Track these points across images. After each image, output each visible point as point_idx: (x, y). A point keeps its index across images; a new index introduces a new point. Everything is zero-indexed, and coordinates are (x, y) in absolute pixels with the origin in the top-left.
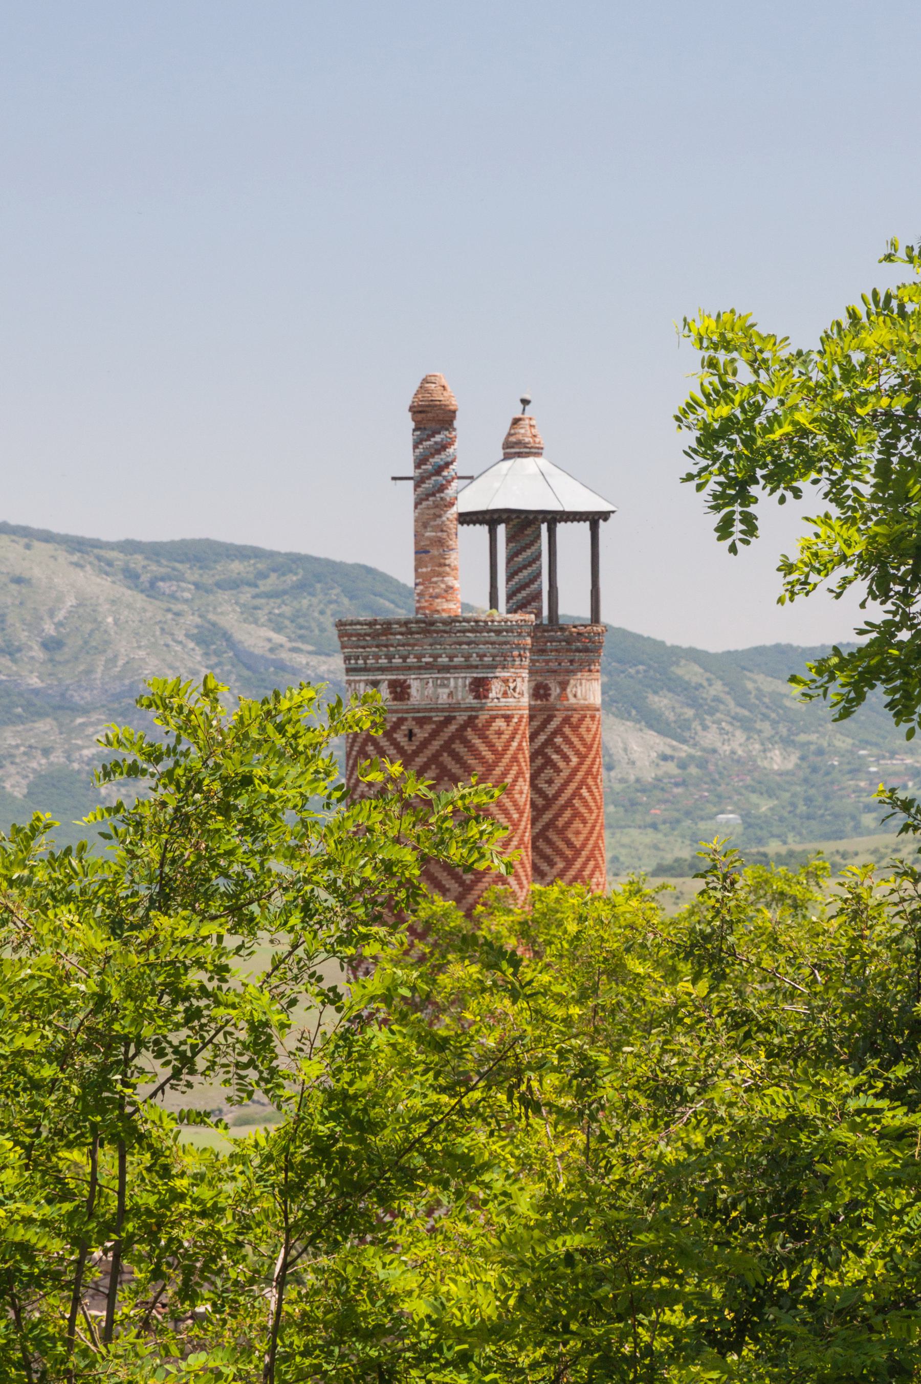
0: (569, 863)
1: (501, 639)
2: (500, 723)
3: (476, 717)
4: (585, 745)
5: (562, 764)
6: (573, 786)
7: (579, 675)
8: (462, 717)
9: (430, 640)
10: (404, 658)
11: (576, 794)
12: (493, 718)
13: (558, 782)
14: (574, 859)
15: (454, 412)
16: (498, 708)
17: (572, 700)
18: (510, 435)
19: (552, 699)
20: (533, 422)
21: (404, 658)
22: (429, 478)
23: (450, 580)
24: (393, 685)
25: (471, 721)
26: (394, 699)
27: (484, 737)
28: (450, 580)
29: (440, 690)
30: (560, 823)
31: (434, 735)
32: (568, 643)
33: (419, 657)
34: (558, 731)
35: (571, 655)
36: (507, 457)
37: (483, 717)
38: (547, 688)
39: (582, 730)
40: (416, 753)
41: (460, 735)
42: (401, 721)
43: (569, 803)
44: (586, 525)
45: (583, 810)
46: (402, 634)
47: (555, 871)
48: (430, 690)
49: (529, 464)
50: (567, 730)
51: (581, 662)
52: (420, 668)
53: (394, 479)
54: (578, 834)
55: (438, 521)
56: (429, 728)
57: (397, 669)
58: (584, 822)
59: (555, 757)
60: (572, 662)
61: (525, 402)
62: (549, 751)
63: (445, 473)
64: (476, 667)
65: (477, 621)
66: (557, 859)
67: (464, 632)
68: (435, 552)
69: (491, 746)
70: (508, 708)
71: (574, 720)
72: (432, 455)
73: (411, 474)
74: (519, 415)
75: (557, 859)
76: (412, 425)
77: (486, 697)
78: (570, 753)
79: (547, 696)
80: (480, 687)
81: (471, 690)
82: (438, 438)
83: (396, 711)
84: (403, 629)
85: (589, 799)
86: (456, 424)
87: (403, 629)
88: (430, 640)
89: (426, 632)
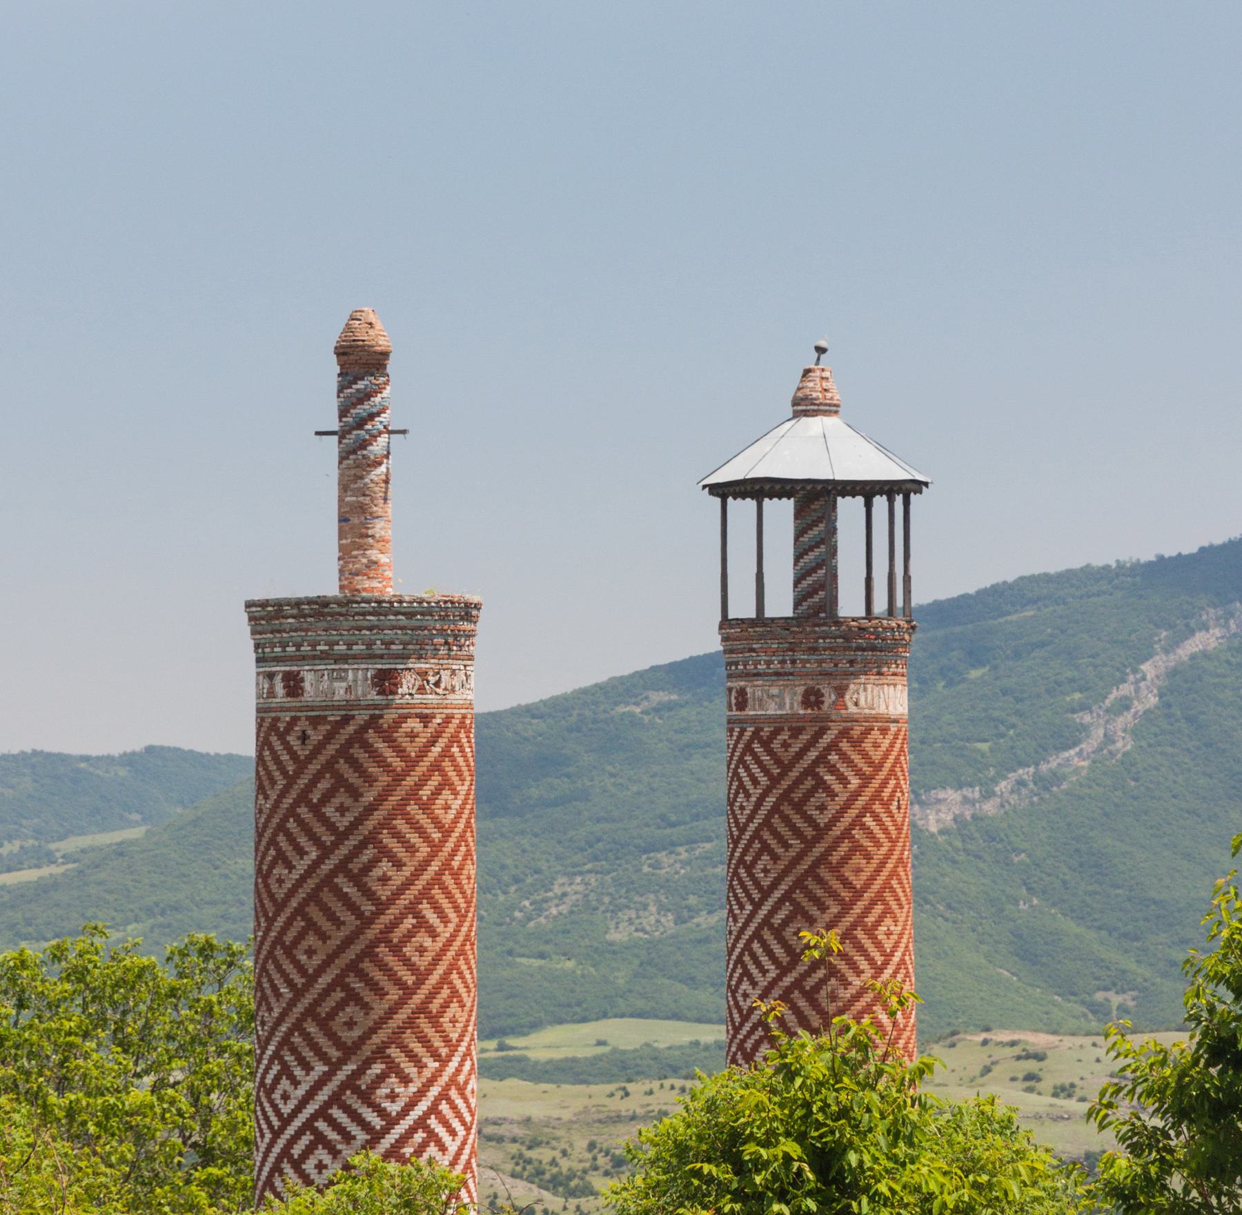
0: (846, 907)
1: (413, 623)
2: (414, 724)
3: (381, 716)
4: (870, 763)
5: (837, 787)
6: (852, 813)
7: (863, 679)
8: (362, 717)
9: (324, 624)
10: (298, 646)
11: (857, 822)
12: (404, 718)
13: (833, 808)
14: (853, 902)
15: (385, 355)
16: (413, 706)
17: (852, 709)
18: (799, 389)
19: (825, 707)
20: (825, 374)
21: (298, 646)
22: (349, 432)
23: (374, 554)
25: (373, 722)
26: (288, 695)
27: (390, 740)
28: (374, 554)
29: (336, 684)
30: (835, 858)
31: (329, 737)
32: (846, 639)
33: (314, 645)
34: (833, 746)
35: (851, 655)
36: (797, 415)
37: (390, 716)
38: (819, 694)
39: (867, 745)
40: (310, 758)
41: (359, 738)
43: (847, 834)
44: (860, 500)
45: (866, 843)
46: (294, 617)
47: (827, 917)
48: (325, 684)
49: (815, 425)
50: (844, 745)
51: (866, 663)
52: (314, 657)
53: (318, 433)
54: (859, 871)
55: (360, 484)
56: (324, 728)
58: (868, 857)
59: (827, 777)
60: (852, 662)
61: (821, 350)
62: (821, 770)
63: (369, 427)
64: (381, 657)
65: (379, 602)
66: (830, 902)
67: (364, 614)
68: (355, 520)
69: (400, 752)
70: (426, 706)
71: (856, 733)
72: (354, 405)
73: (336, 428)
74: (812, 366)
75: (830, 902)
76: (338, 369)
77: (396, 693)
78: (849, 773)
79: (819, 703)
80: (386, 681)
81: (374, 685)
82: (360, 385)
83: (289, 710)
84: (295, 611)
85: (876, 829)
86: (390, 369)
87: (295, 611)
88: (324, 624)
89: (318, 615)
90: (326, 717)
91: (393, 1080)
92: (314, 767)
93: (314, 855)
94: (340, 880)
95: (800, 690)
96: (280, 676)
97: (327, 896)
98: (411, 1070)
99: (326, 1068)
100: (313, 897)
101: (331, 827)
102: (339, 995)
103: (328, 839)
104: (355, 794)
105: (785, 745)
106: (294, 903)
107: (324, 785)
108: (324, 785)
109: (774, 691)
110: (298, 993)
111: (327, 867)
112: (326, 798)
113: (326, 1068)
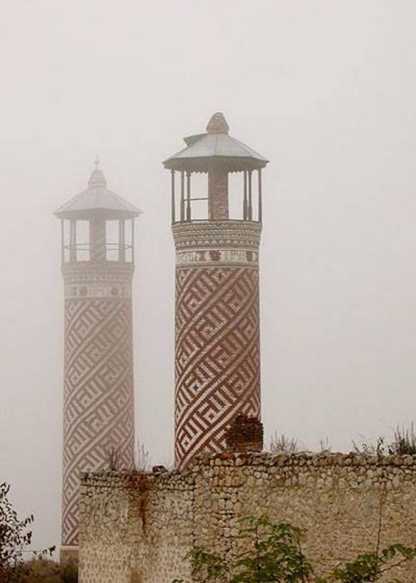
10: (218, 241)
21: (218, 241)
24: (212, 253)
42: (216, 270)
50: (245, 276)
52: (203, 246)
56: (229, 273)
57: (215, 246)
66: (120, 367)
79: (116, 294)
90: (229, 269)
92: (225, 288)
93: (225, 322)
95: (110, 288)
96: (208, 253)
98: (219, 406)
99: (231, 405)
101: (233, 311)
103: (231, 316)
104: (240, 298)
105: (105, 308)
107: (229, 295)
108: (229, 295)
109: (100, 288)
111: (230, 327)
112: (230, 300)
113: (231, 405)
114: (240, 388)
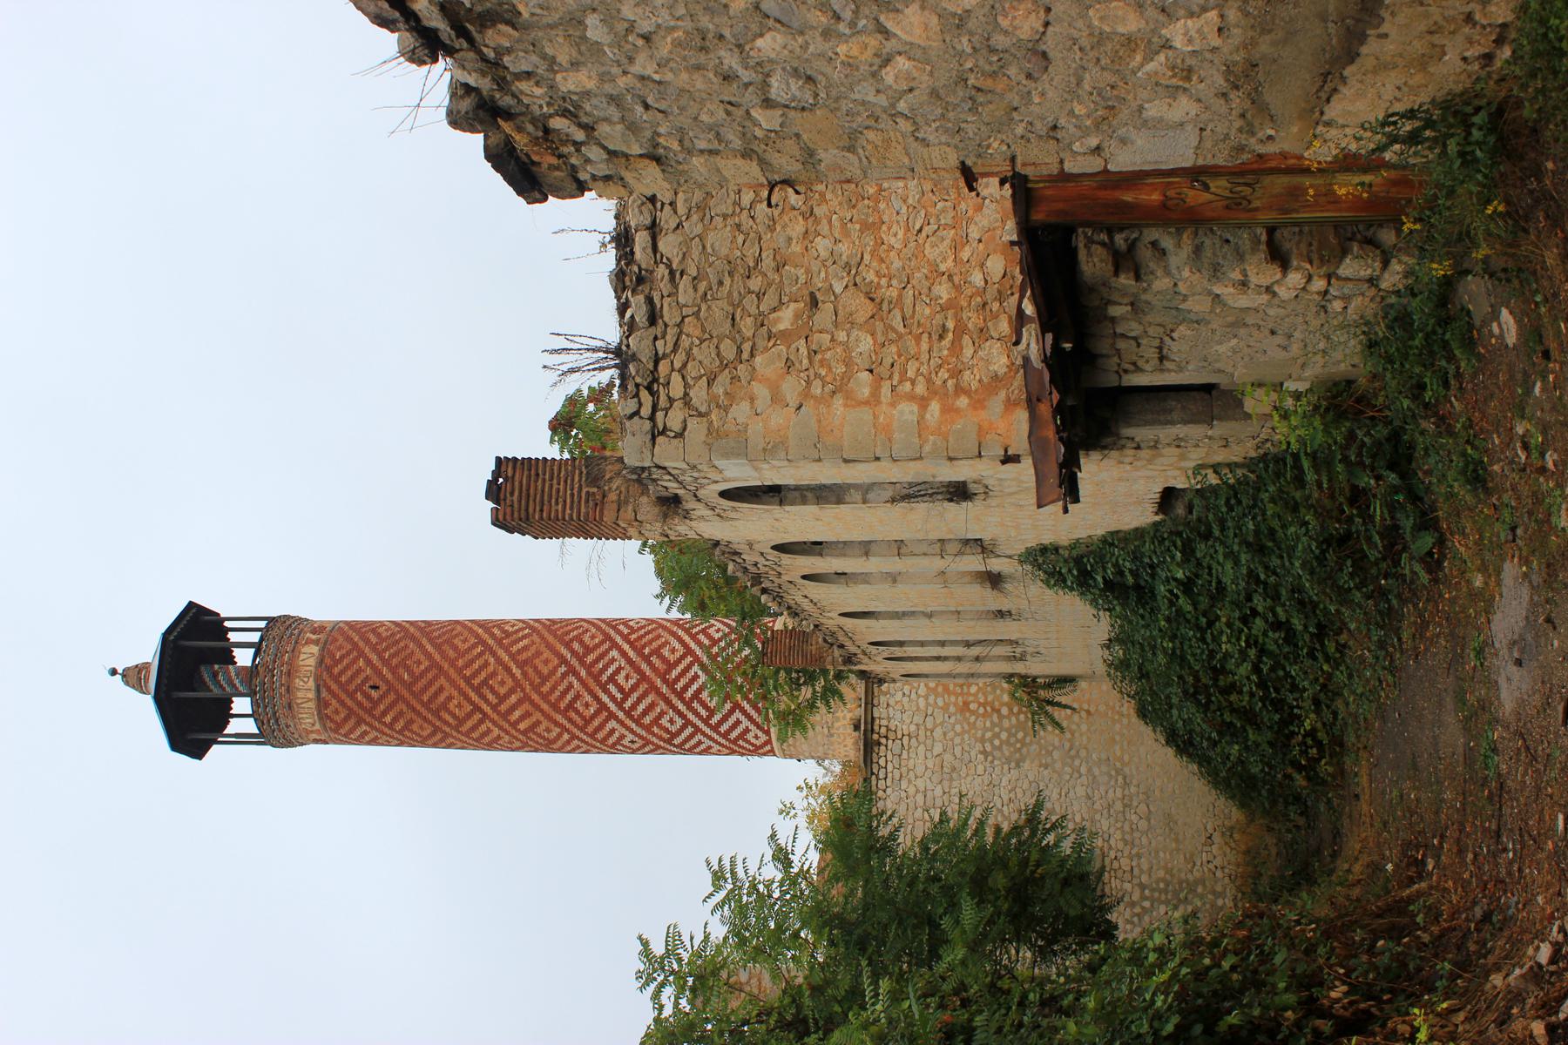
15: (191, 605)
23: (880, 804)
91: (537, 661)
94: (336, 671)
97: (636, 714)
100: (638, 722)
102: (695, 704)
106: (643, 733)
110: (697, 730)
114: (671, 721)
